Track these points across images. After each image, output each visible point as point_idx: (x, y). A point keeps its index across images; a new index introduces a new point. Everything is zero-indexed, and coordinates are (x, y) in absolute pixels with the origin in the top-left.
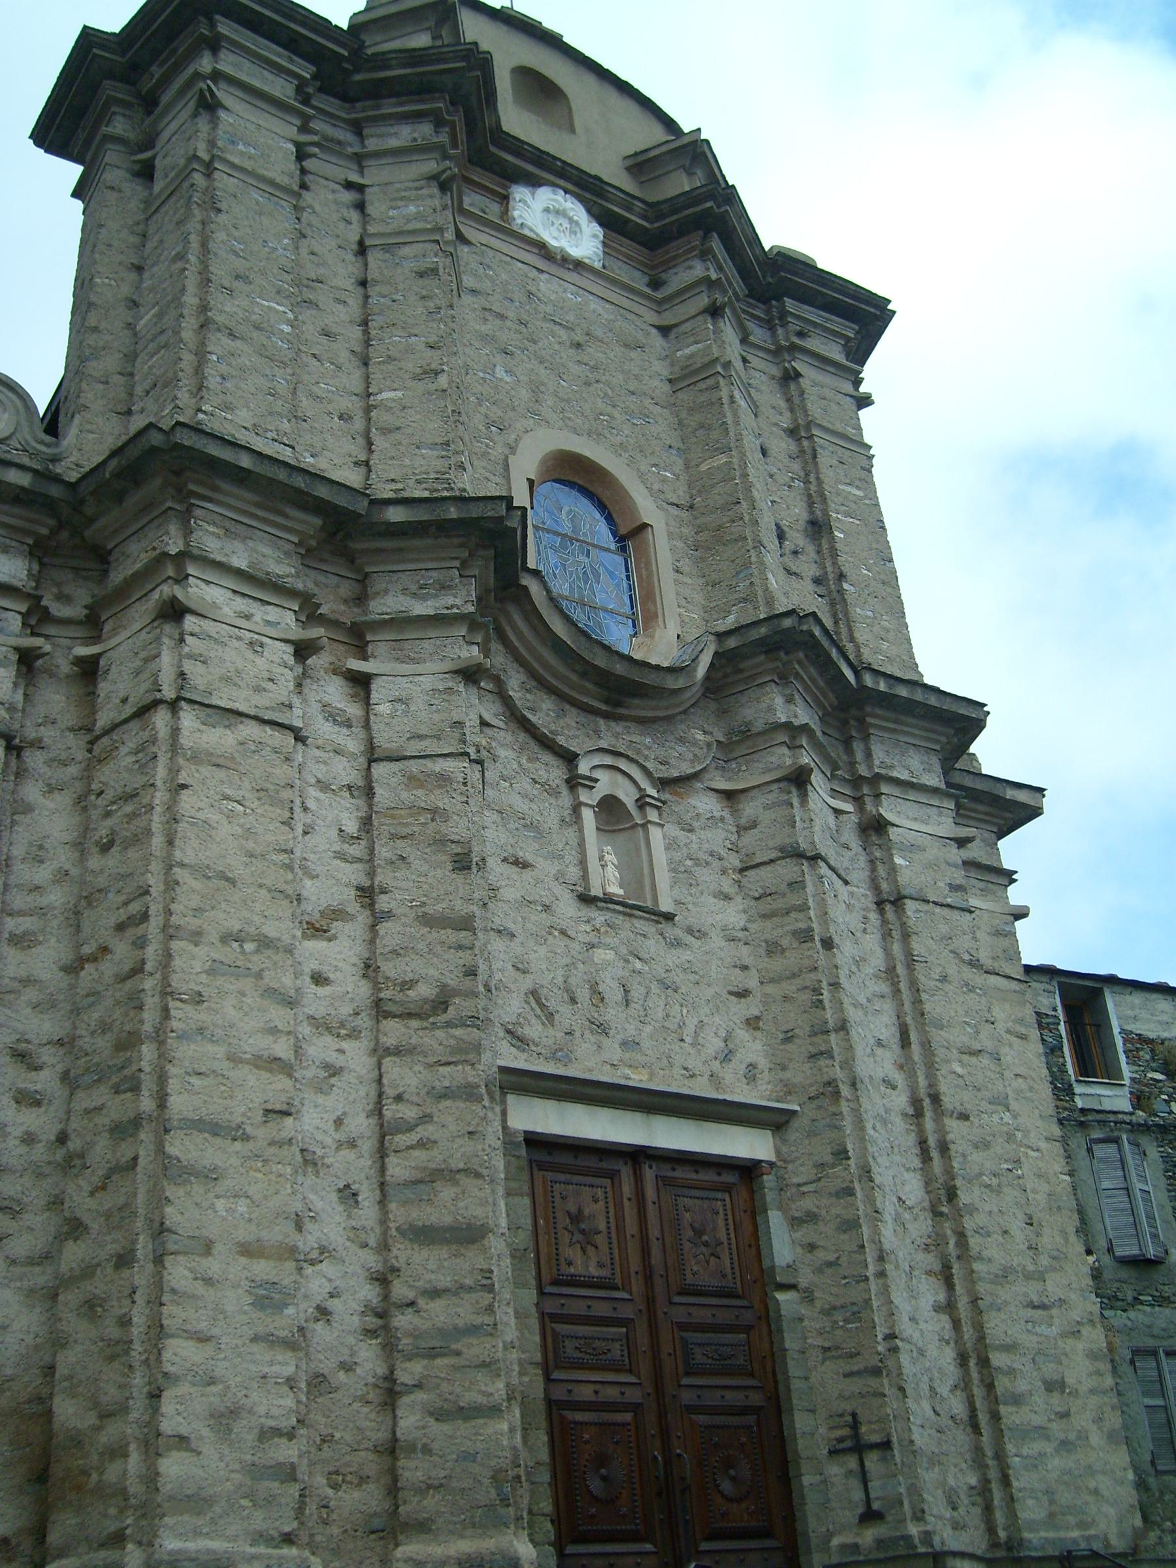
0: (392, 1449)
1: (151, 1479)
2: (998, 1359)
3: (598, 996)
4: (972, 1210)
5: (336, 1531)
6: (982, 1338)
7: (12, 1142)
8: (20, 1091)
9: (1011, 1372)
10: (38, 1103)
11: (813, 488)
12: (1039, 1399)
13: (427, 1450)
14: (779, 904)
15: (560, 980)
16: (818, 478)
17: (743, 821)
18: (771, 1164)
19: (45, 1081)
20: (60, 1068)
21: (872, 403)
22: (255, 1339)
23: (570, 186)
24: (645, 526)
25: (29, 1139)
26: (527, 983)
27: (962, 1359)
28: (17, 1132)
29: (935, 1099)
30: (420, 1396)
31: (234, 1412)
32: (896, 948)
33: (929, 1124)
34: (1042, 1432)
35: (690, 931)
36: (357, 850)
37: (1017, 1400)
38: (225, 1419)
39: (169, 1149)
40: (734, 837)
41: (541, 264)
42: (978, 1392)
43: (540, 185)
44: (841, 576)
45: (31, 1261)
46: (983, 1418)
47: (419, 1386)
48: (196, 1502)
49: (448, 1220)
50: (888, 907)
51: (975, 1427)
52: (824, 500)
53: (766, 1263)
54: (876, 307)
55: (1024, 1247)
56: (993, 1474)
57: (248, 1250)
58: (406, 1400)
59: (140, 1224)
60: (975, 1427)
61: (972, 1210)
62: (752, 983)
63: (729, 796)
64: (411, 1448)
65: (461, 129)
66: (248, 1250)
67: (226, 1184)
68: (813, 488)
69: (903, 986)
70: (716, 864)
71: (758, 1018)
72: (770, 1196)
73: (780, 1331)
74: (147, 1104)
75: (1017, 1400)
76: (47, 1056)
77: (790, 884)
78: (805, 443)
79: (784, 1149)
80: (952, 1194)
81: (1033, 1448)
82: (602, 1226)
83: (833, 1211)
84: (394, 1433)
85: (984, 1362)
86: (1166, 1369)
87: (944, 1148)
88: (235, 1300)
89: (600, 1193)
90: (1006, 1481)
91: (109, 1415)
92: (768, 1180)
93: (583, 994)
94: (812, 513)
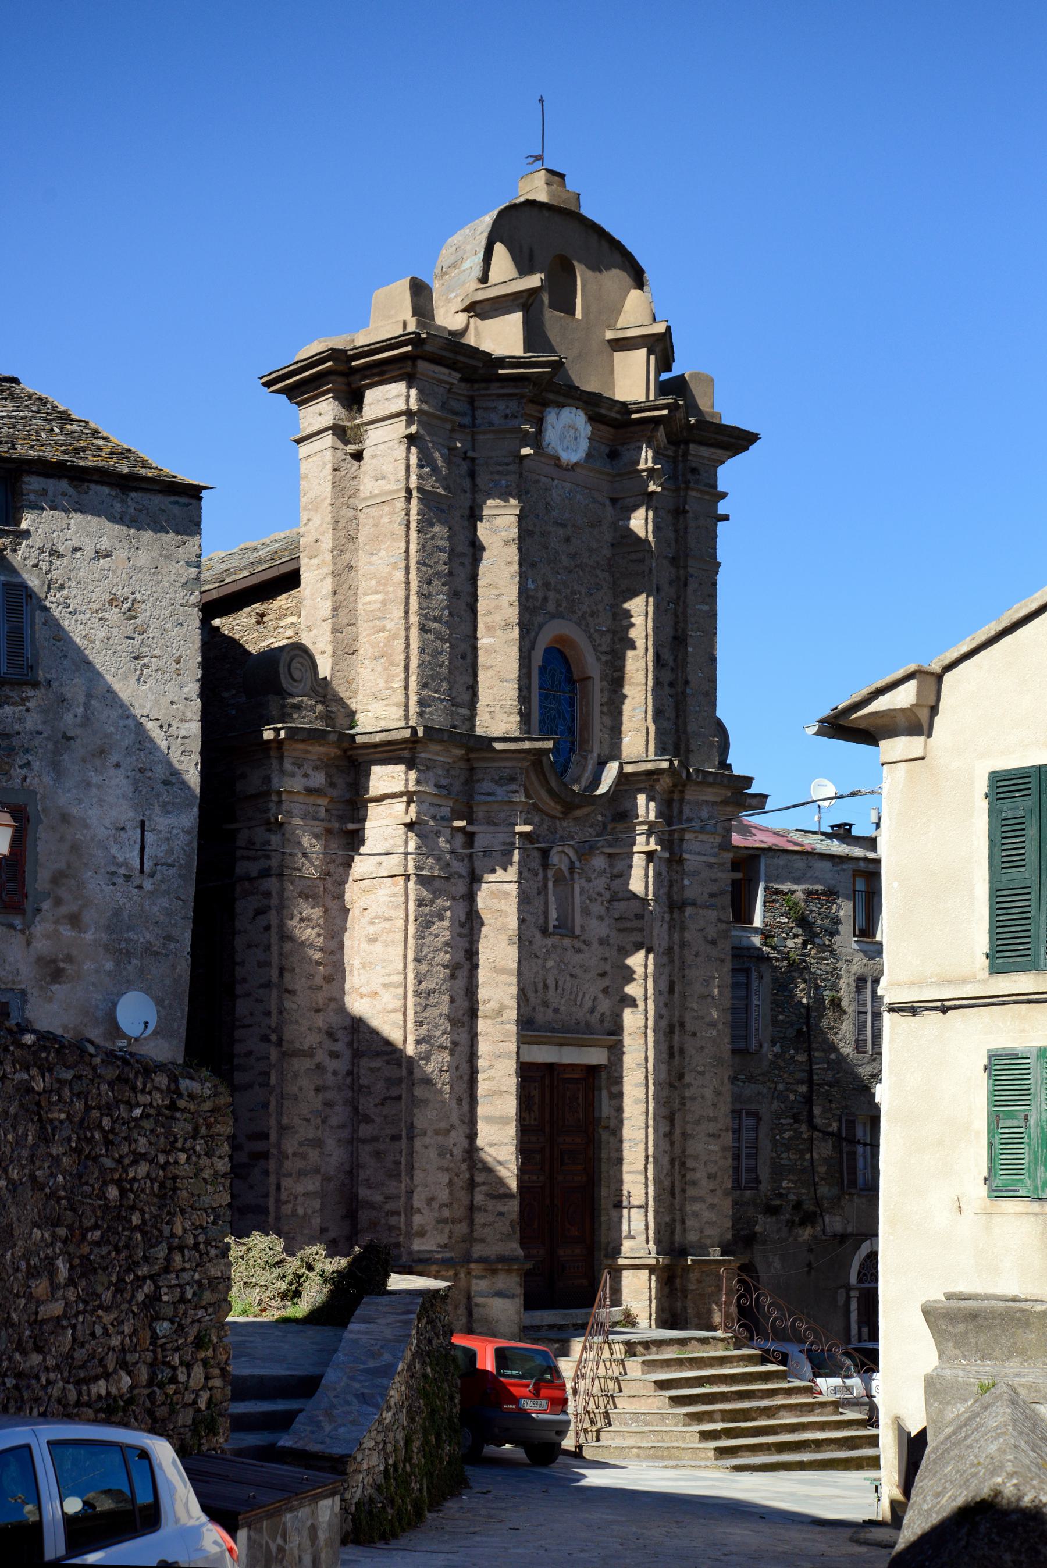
0: (472, 1208)
1: (409, 1224)
2: (690, 1163)
3: (546, 987)
4: (689, 1085)
6: (684, 1151)
7: (329, 1075)
8: (331, 1051)
9: (693, 1170)
10: (337, 1057)
11: (680, 610)
12: (704, 1182)
13: (486, 1211)
14: (628, 925)
16: (684, 602)
17: (615, 871)
18: (606, 1066)
19: (339, 1046)
20: (346, 1040)
24: (589, 678)
25: (335, 1073)
27: (672, 1161)
28: (330, 1069)
29: (682, 1025)
30: (483, 1188)
32: (676, 936)
33: (676, 1038)
34: (701, 1199)
36: (465, 931)
37: (694, 1183)
38: (430, 1200)
39: (416, 1093)
40: (608, 881)
42: (677, 1177)
43: (563, 407)
44: (687, 682)
45: (338, 1127)
46: (677, 1190)
47: (484, 1184)
49: (498, 1113)
50: (676, 910)
51: (673, 1194)
52: (686, 622)
53: (597, 1115)
55: (710, 1104)
56: (678, 1217)
58: (478, 1189)
59: (403, 1124)
60: (673, 1194)
61: (689, 1085)
62: (608, 968)
63: (610, 855)
64: (479, 1209)
68: (680, 610)
69: (676, 958)
70: (600, 899)
71: (608, 987)
72: (604, 1083)
73: (600, 1148)
74: (404, 1072)
75: (694, 1183)
76: (340, 1034)
77: (636, 915)
78: (682, 572)
79: (612, 1058)
80: (681, 1076)
81: (697, 1207)
83: (634, 1093)
84: (472, 1201)
85: (683, 1164)
86: (744, 1123)
87: (682, 1051)
88: (433, 1154)
90: (683, 1222)
91: (390, 1198)
92: (604, 1075)
93: (540, 986)
94: (676, 630)
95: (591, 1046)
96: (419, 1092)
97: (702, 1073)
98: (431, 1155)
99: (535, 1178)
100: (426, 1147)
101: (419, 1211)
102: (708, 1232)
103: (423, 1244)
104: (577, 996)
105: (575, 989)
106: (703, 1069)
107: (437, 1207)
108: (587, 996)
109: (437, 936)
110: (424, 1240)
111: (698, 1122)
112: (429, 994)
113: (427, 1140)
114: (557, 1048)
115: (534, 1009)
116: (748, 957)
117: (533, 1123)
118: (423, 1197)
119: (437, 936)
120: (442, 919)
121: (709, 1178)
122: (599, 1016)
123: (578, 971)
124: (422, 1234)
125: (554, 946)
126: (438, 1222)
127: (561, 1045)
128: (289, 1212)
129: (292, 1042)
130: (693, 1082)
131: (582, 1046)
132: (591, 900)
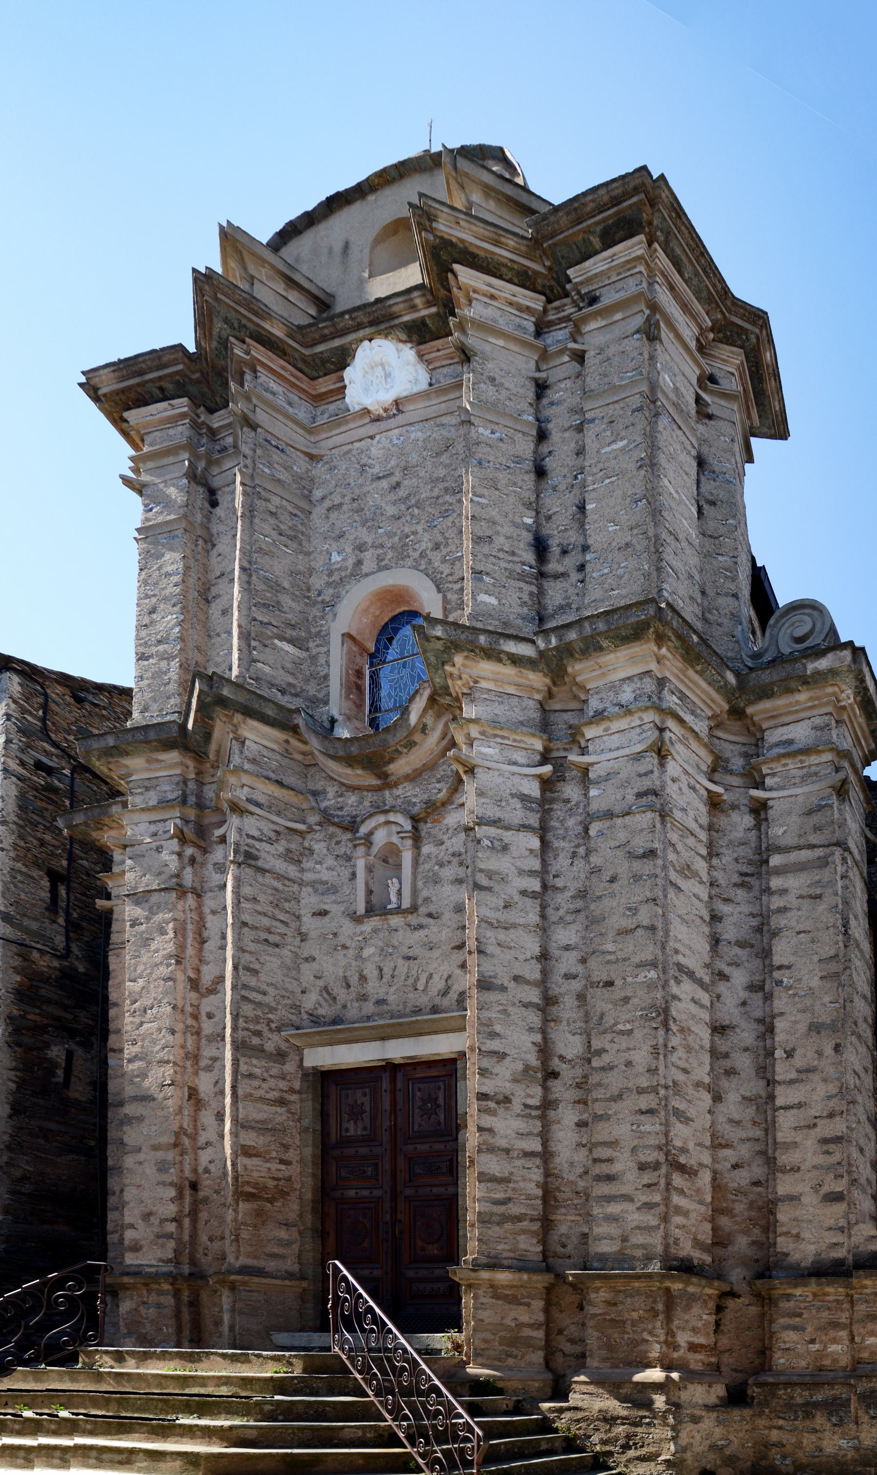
3: (363, 978)
5: (210, 1258)
15: (341, 974)
21: (91, 386)
22: (158, 1184)
23: (368, 331)
26: (321, 983)
31: (150, 1214)
34: (628, 1198)
35: (430, 915)
38: (147, 1216)
41: (372, 429)
48: (136, 1248)
54: (636, 190)
57: (156, 1148)
65: (269, 358)
66: (156, 1148)
67: (147, 1121)
70: (455, 860)
82: (417, 1111)
88: (150, 1170)
89: (367, 1091)
95: (436, 1032)
96: (11, 1098)
97: (630, 1032)
98: (148, 1171)
99: (366, 1193)
100: (140, 1163)
101: (132, 1226)
102: (638, 1239)
103: (137, 1258)
104: (417, 979)
105: (414, 972)
106: (628, 1027)
107: (157, 1222)
108: (436, 977)
109: (156, 951)
110: (139, 1254)
111: (618, 1097)
112: (145, 1011)
113: (141, 1156)
114: (378, 1043)
115: (344, 1007)
116: (201, 784)
117: (359, 1133)
118: (137, 1212)
119: (156, 951)
120: (163, 932)
121: (639, 1169)
122: (455, 996)
123: (416, 951)
124: (136, 1248)
125: (375, 931)
126: (158, 1236)
127: (383, 1039)
128: (116, 1241)
129: (118, 1094)
130: (608, 1046)
131: (421, 1034)
132: (441, 865)
